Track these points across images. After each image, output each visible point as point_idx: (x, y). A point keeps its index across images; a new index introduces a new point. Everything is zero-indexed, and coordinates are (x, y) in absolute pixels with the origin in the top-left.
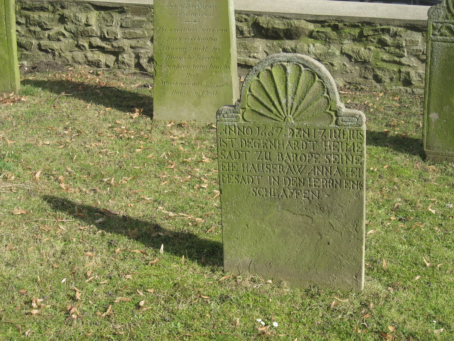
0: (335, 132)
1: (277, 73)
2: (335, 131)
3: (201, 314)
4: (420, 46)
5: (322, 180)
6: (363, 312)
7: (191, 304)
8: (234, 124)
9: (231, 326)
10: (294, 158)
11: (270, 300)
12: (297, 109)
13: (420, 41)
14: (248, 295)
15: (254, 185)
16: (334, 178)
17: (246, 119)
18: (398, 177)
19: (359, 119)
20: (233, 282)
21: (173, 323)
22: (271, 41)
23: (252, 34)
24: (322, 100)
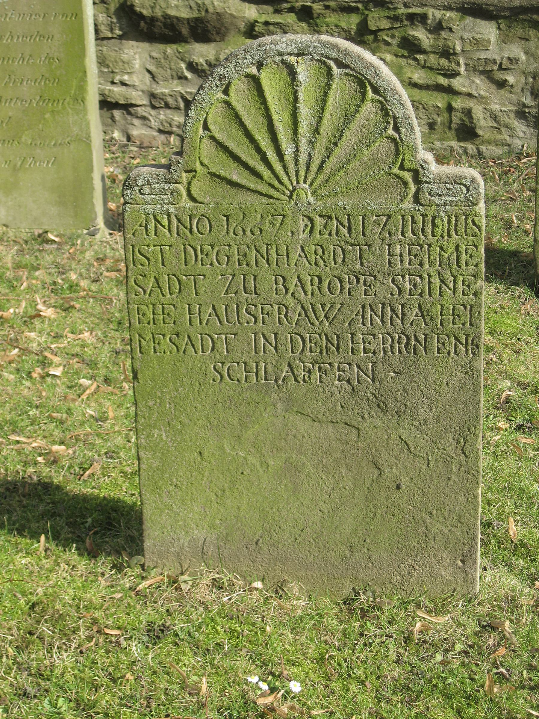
0: (414, 222)
1: (271, 82)
2: (413, 217)
3: (110, 674)
4: (494, 52)
5: (381, 336)
6: (491, 642)
7: (81, 652)
8: (168, 210)
9: (188, 698)
10: (315, 288)
11: (268, 629)
12: (321, 168)
13: (493, 39)
14: (212, 620)
15: (218, 356)
16: (411, 332)
17: (195, 195)
18: (491, 333)
19: (471, 188)
20: (171, 593)
21: (46, 701)
22: (161, 46)
23: (118, 32)
24: (382, 146)
